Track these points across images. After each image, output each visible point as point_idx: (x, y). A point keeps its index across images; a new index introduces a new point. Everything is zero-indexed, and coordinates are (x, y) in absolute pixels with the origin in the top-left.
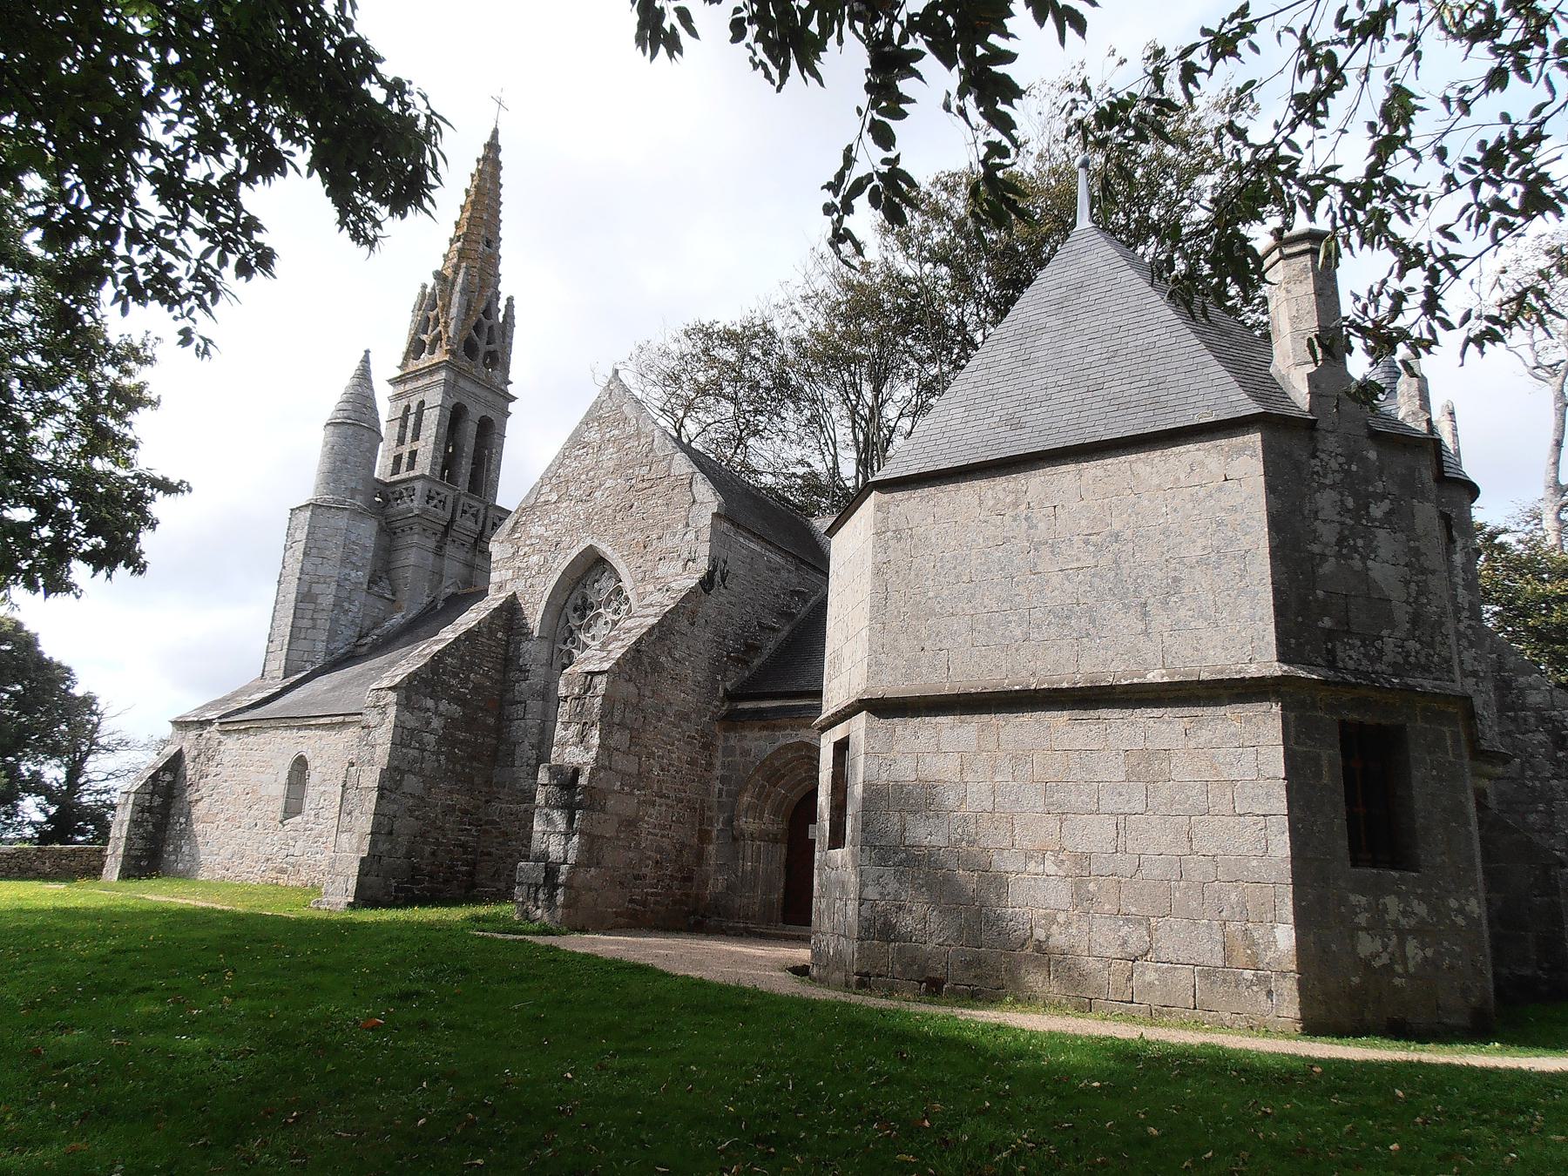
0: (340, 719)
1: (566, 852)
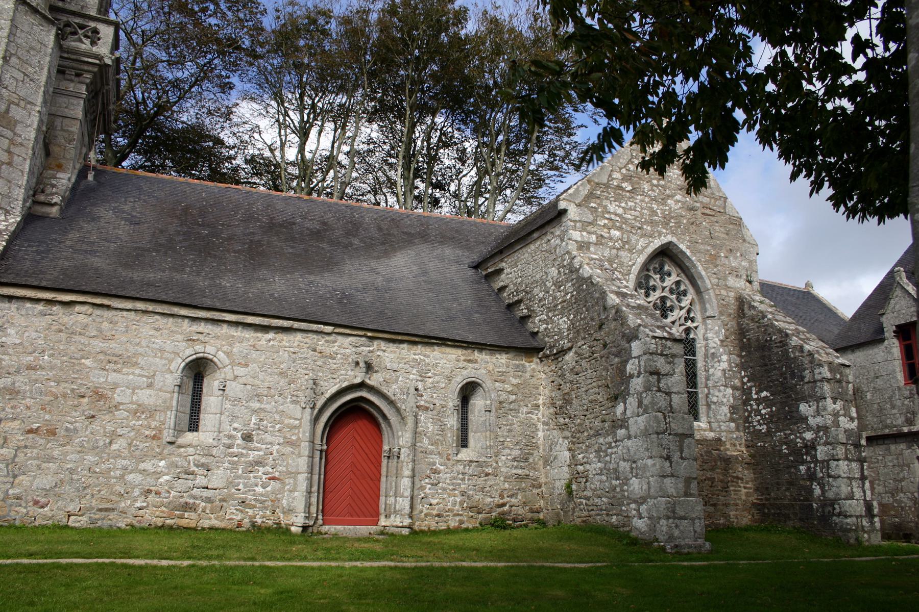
0: (286, 323)
1: (864, 492)
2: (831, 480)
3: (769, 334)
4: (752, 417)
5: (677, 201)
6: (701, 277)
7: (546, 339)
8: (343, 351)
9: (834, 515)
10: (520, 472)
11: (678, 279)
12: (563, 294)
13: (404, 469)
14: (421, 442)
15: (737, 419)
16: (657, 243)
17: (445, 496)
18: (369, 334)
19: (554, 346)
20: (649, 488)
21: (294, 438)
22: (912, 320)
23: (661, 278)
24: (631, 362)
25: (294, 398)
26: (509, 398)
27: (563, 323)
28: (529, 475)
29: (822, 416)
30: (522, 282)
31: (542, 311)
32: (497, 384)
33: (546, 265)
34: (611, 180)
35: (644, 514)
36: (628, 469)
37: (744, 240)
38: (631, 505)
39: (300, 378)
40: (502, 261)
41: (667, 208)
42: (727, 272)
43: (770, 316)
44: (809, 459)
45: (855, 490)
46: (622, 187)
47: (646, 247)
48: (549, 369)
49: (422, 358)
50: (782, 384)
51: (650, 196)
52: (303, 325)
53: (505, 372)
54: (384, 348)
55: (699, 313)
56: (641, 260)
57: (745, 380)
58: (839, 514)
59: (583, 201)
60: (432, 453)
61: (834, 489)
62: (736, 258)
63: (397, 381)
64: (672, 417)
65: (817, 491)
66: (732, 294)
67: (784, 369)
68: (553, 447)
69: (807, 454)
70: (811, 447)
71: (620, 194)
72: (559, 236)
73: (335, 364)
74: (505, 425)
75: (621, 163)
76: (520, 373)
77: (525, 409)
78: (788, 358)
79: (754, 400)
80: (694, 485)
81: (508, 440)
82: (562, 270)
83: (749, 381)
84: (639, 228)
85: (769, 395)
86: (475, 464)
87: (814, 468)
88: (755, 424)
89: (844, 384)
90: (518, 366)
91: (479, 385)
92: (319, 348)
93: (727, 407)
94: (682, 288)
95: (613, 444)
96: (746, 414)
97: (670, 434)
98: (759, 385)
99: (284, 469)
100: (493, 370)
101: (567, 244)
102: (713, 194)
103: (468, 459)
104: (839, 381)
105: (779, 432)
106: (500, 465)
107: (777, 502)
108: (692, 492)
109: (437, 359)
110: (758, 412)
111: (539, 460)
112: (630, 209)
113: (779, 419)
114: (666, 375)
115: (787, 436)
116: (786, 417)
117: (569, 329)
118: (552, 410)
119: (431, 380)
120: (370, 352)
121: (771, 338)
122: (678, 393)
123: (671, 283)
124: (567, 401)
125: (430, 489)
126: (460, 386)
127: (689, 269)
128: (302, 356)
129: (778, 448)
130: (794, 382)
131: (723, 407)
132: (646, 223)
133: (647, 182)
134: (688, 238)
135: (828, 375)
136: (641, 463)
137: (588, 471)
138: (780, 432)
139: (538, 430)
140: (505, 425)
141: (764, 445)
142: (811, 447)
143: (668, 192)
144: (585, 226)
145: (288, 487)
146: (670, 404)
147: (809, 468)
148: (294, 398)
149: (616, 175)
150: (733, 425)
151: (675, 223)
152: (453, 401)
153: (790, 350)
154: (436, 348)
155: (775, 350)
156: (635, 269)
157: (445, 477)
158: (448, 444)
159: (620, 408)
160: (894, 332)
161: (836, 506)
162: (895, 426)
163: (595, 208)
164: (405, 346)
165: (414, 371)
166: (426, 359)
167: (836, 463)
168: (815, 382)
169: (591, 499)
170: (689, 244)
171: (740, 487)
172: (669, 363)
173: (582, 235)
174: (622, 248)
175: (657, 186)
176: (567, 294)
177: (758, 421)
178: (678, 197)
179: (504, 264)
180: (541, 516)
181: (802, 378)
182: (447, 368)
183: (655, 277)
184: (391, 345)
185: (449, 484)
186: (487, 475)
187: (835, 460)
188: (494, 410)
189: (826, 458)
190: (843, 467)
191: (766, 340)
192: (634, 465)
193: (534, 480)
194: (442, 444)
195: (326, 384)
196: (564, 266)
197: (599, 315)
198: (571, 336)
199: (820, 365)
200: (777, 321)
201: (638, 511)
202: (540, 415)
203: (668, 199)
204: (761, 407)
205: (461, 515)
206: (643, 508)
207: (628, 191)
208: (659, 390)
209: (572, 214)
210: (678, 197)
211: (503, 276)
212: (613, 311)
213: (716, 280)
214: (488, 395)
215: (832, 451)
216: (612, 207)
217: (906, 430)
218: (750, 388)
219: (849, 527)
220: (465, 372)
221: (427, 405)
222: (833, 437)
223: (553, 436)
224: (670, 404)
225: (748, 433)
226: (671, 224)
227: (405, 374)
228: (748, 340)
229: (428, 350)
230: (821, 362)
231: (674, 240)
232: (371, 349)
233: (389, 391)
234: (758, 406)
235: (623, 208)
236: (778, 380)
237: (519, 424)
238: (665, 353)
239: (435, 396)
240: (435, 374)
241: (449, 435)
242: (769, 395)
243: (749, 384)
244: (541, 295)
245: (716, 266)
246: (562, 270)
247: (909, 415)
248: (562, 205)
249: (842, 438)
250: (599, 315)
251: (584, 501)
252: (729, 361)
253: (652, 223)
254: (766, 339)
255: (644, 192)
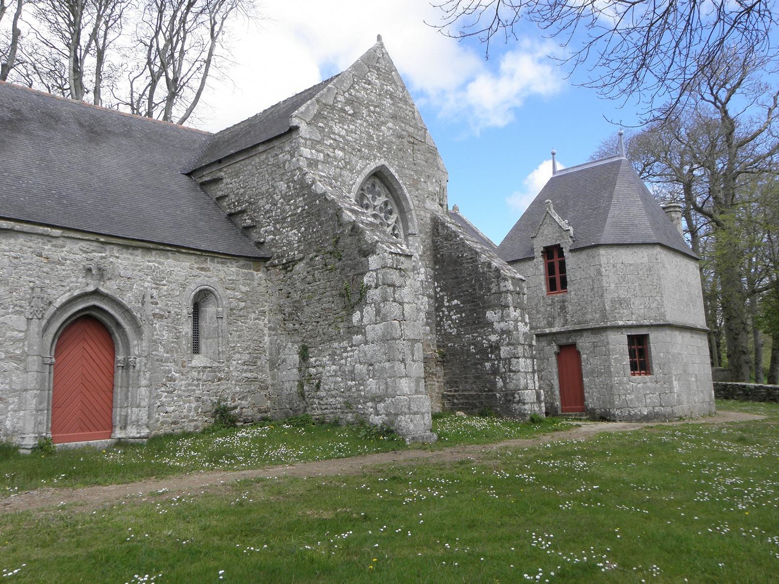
1: (534, 383)
2: (512, 374)
3: (461, 252)
4: (443, 322)
5: (389, 128)
6: (406, 199)
7: (273, 249)
8: (72, 256)
9: (514, 402)
10: (249, 375)
11: (387, 199)
12: (292, 207)
13: (141, 378)
14: (157, 351)
15: (431, 323)
16: (372, 166)
17: (181, 403)
18: (102, 239)
19: (283, 256)
20: (387, 388)
21: (18, 352)
22: (557, 243)
23: (373, 197)
24: (368, 274)
25: (17, 308)
26: (239, 305)
27: (293, 235)
28: (257, 378)
29: (506, 322)
30: (245, 192)
31: (269, 223)
32: (229, 291)
33: (273, 179)
34: (336, 103)
35: (382, 411)
36: (365, 371)
37: (438, 168)
38: (368, 404)
39: (24, 286)
40: (220, 170)
41: (381, 134)
42: (426, 196)
43: (462, 236)
44: (493, 356)
45: (529, 381)
46: (345, 110)
47: (364, 169)
48: (277, 278)
49: (156, 265)
50: (472, 294)
51: (367, 121)
52: (26, 227)
53: (235, 280)
54: (117, 255)
55: (402, 230)
56: (360, 180)
57: (438, 290)
58: (519, 402)
59: (312, 120)
60: (167, 360)
61: (514, 381)
62: (432, 183)
63: (131, 288)
64: (406, 324)
65: (500, 383)
66: (428, 215)
67: (474, 281)
68: (281, 351)
69: (492, 353)
70: (495, 348)
71: (343, 117)
72: (289, 152)
73: (64, 270)
74: (235, 331)
75: (345, 87)
76: (249, 282)
77: (253, 316)
78: (477, 272)
79: (445, 307)
80: (422, 384)
81: (239, 345)
82: (291, 185)
83: (441, 291)
84: (359, 150)
85: (459, 303)
86: (208, 369)
87: (498, 364)
88: (446, 327)
89: (521, 295)
90: (247, 274)
91: (211, 292)
92: (45, 253)
93: (424, 313)
94: (389, 208)
95: (349, 349)
96: (438, 319)
97: (404, 340)
98: (451, 295)
99: (7, 387)
100: (224, 278)
101: (298, 160)
102: (416, 124)
103: (202, 365)
104: (518, 293)
105: (467, 334)
106: (231, 369)
107: (465, 393)
108: (421, 389)
109: (171, 267)
110: (449, 317)
111: (266, 363)
112: (351, 132)
113: (467, 324)
114: (400, 287)
115: (474, 338)
116: (474, 322)
117: (299, 241)
118: (280, 317)
119: (165, 288)
120: (102, 258)
121: (463, 255)
122: (409, 303)
123: (380, 202)
124: (298, 307)
125: (166, 397)
126: (193, 293)
127: (396, 191)
128: (26, 261)
129: (466, 348)
130: (482, 293)
131: (421, 313)
132: (364, 146)
133: (366, 108)
134: (396, 163)
135: (511, 288)
136: (378, 366)
137: (321, 373)
138: (469, 334)
139: (264, 335)
140: (235, 331)
141: (454, 345)
142: (495, 348)
143: (382, 119)
144: (314, 144)
145: (12, 406)
146: (403, 312)
147: (493, 365)
148: (17, 308)
149: (340, 98)
150: (428, 328)
151: (387, 148)
152: (187, 310)
153: (480, 266)
154: (170, 254)
155: (466, 266)
156: (355, 188)
157: (181, 384)
158: (183, 351)
159: (356, 316)
160: (542, 252)
161: (516, 396)
162: (539, 328)
163: (322, 127)
164: (139, 252)
165: (149, 279)
166: (160, 266)
167: (516, 360)
168: (501, 293)
169: (324, 399)
170: (397, 168)
171: (434, 381)
172: (402, 276)
173: (311, 152)
174: (345, 167)
175: (374, 112)
176: (298, 208)
177: (449, 325)
178: (390, 125)
179: (223, 174)
180: (269, 414)
181: (489, 290)
182: (182, 276)
183: (368, 196)
184: (124, 250)
185: (184, 391)
186: (220, 379)
187: (515, 358)
188: (225, 317)
189: (509, 356)
190: (523, 364)
191: (458, 257)
192: (371, 368)
193: (262, 382)
194: (177, 352)
195: (54, 292)
196: (294, 181)
197: (334, 229)
198: (302, 247)
199: (505, 279)
200: (467, 240)
201: (375, 409)
202: (266, 321)
203: (382, 126)
204: (452, 313)
205: (196, 420)
206: (381, 406)
207: (350, 115)
208: (394, 301)
209: (304, 131)
210: (390, 125)
211: (222, 186)
212: (350, 227)
213: (417, 202)
214: (220, 302)
215: (514, 351)
216: (337, 129)
217: (547, 331)
218: (442, 297)
219: (526, 412)
220: (198, 280)
221: (163, 313)
222: (514, 339)
223: (281, 341)
224: (403, 312)
225: (439, 335)
226: (384, 149)
227: (140, 282)
228: (442, 255)
229: (163, 257)
230: (506, 277)
231: (386, 164)
232: (104, 255)
233: (127, 299)
234: (449, 312)
235: (346, 130)
236: (467, 291)
237: (248, 330)
238: (399, 267)
239: (170, 303)
240: (170, 282)
241: (184, 342)
242: (459, 303)
243: (441, 294)
244: (268, 207)
245: (417, 190)
246: (291, 185)
247: (550, 319)
248: (295, 122)
249: (522, 340)
250: (334, 229)
251: (317, 401)
252: (426, 273)
253: (370, 147)
254: (458, 256)
255: (362, 116)
